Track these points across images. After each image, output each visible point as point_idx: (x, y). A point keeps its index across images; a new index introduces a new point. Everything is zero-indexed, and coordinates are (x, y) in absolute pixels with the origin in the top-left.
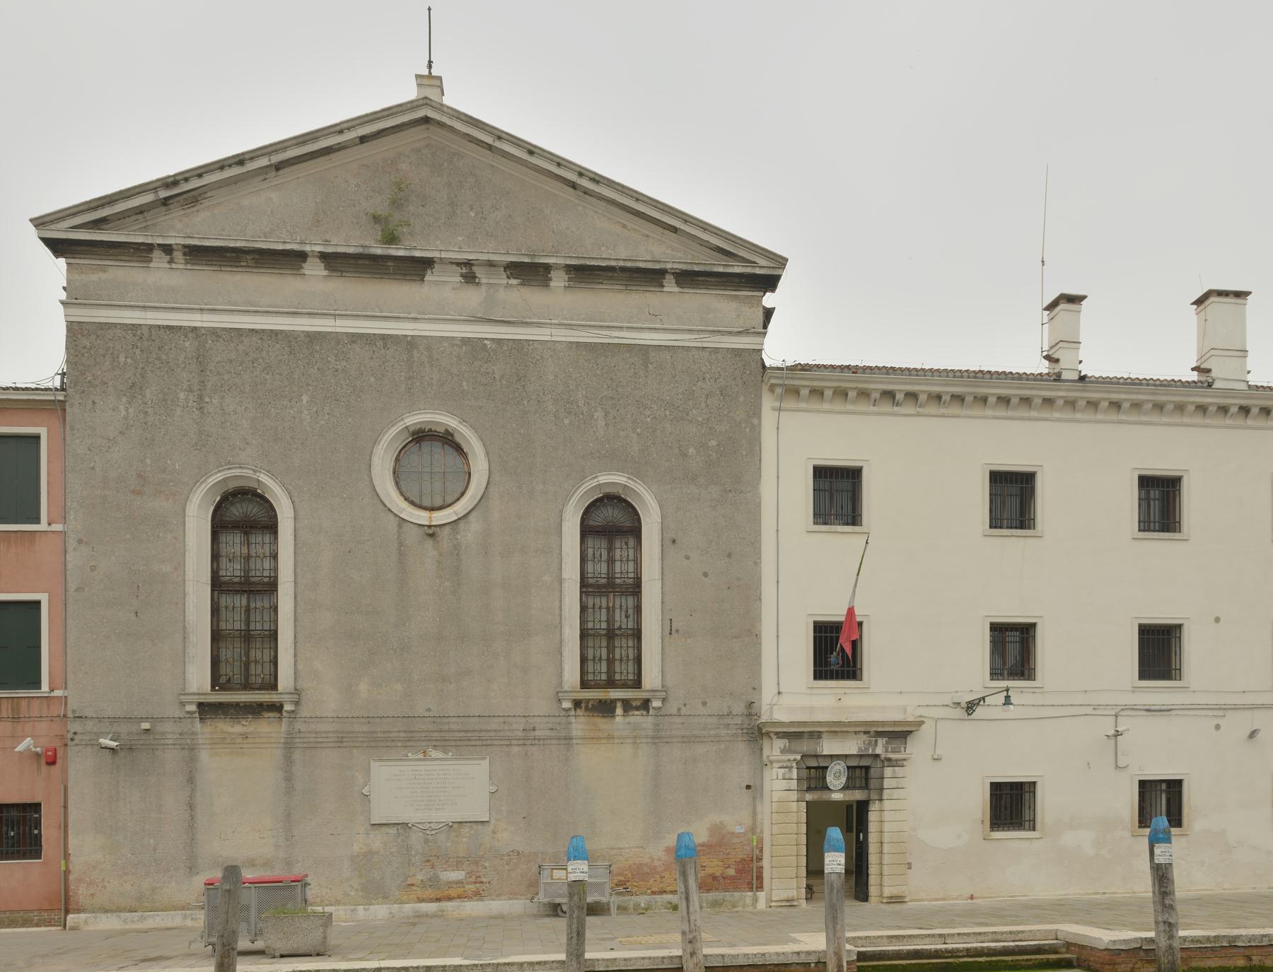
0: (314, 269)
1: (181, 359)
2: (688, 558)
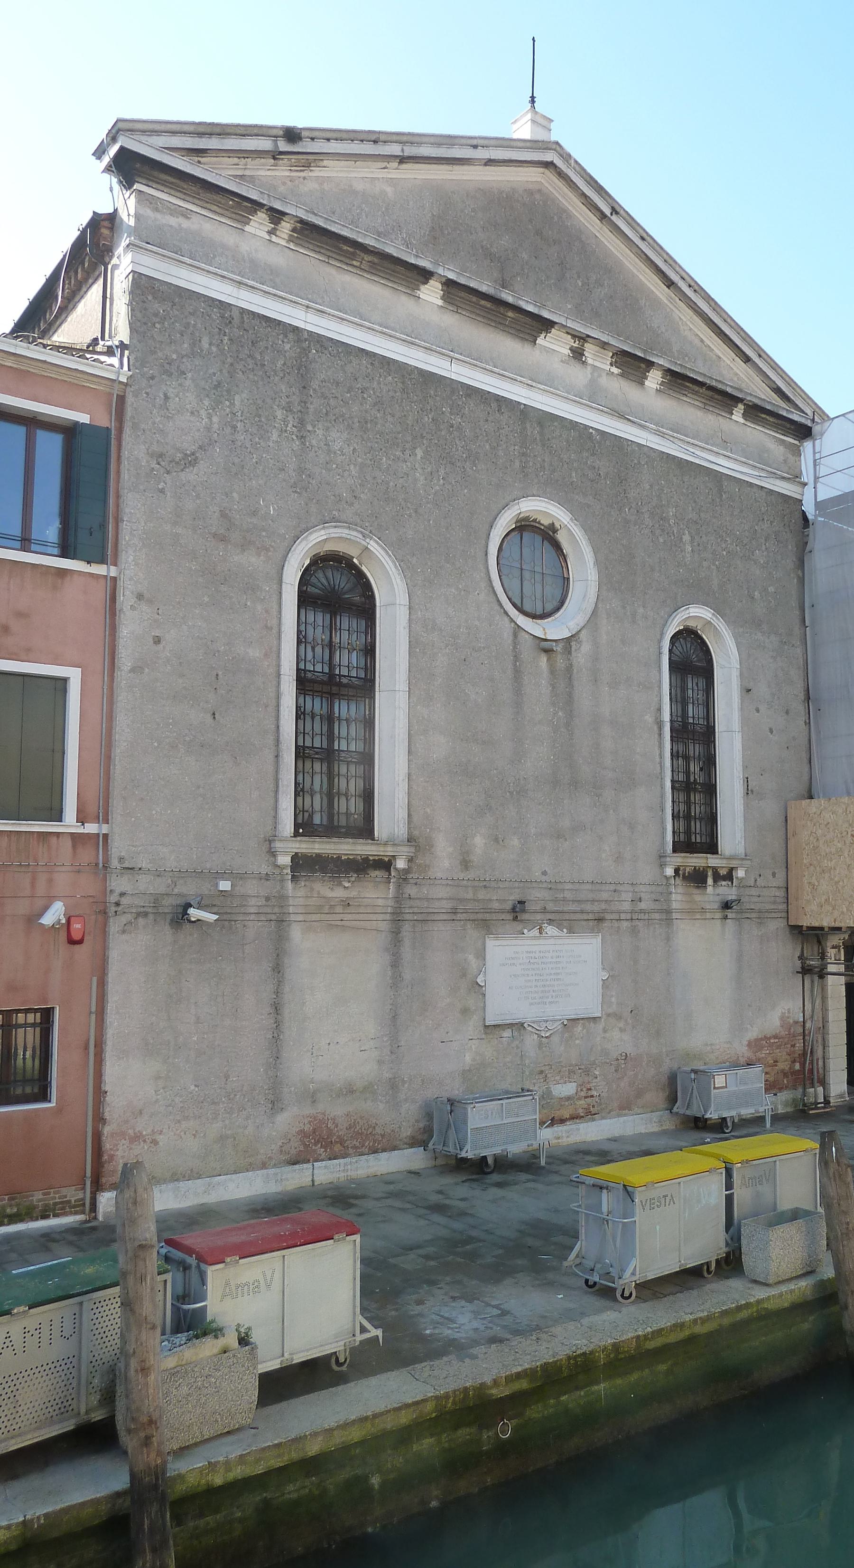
0: (431, 294)
1: (280, 364)
2: (758, 711)
